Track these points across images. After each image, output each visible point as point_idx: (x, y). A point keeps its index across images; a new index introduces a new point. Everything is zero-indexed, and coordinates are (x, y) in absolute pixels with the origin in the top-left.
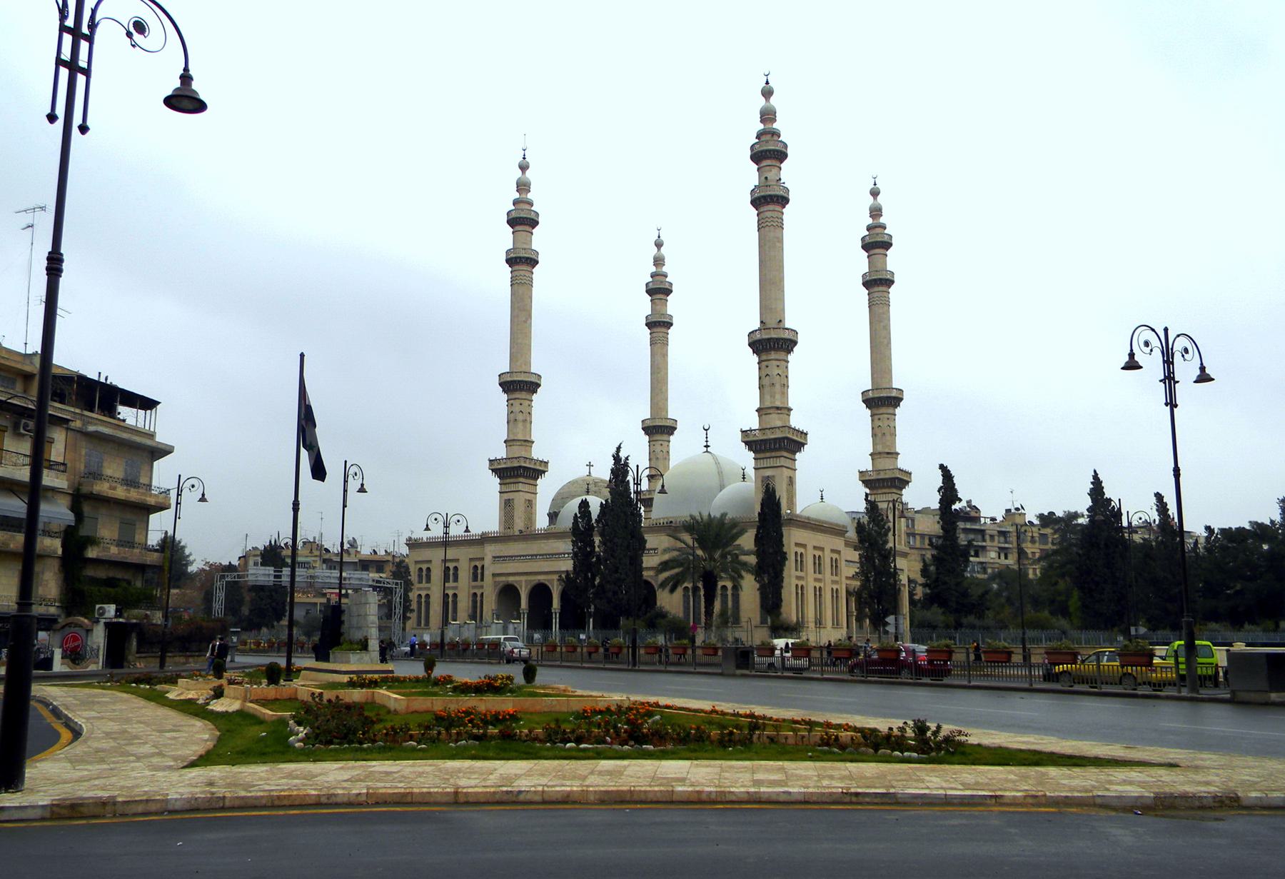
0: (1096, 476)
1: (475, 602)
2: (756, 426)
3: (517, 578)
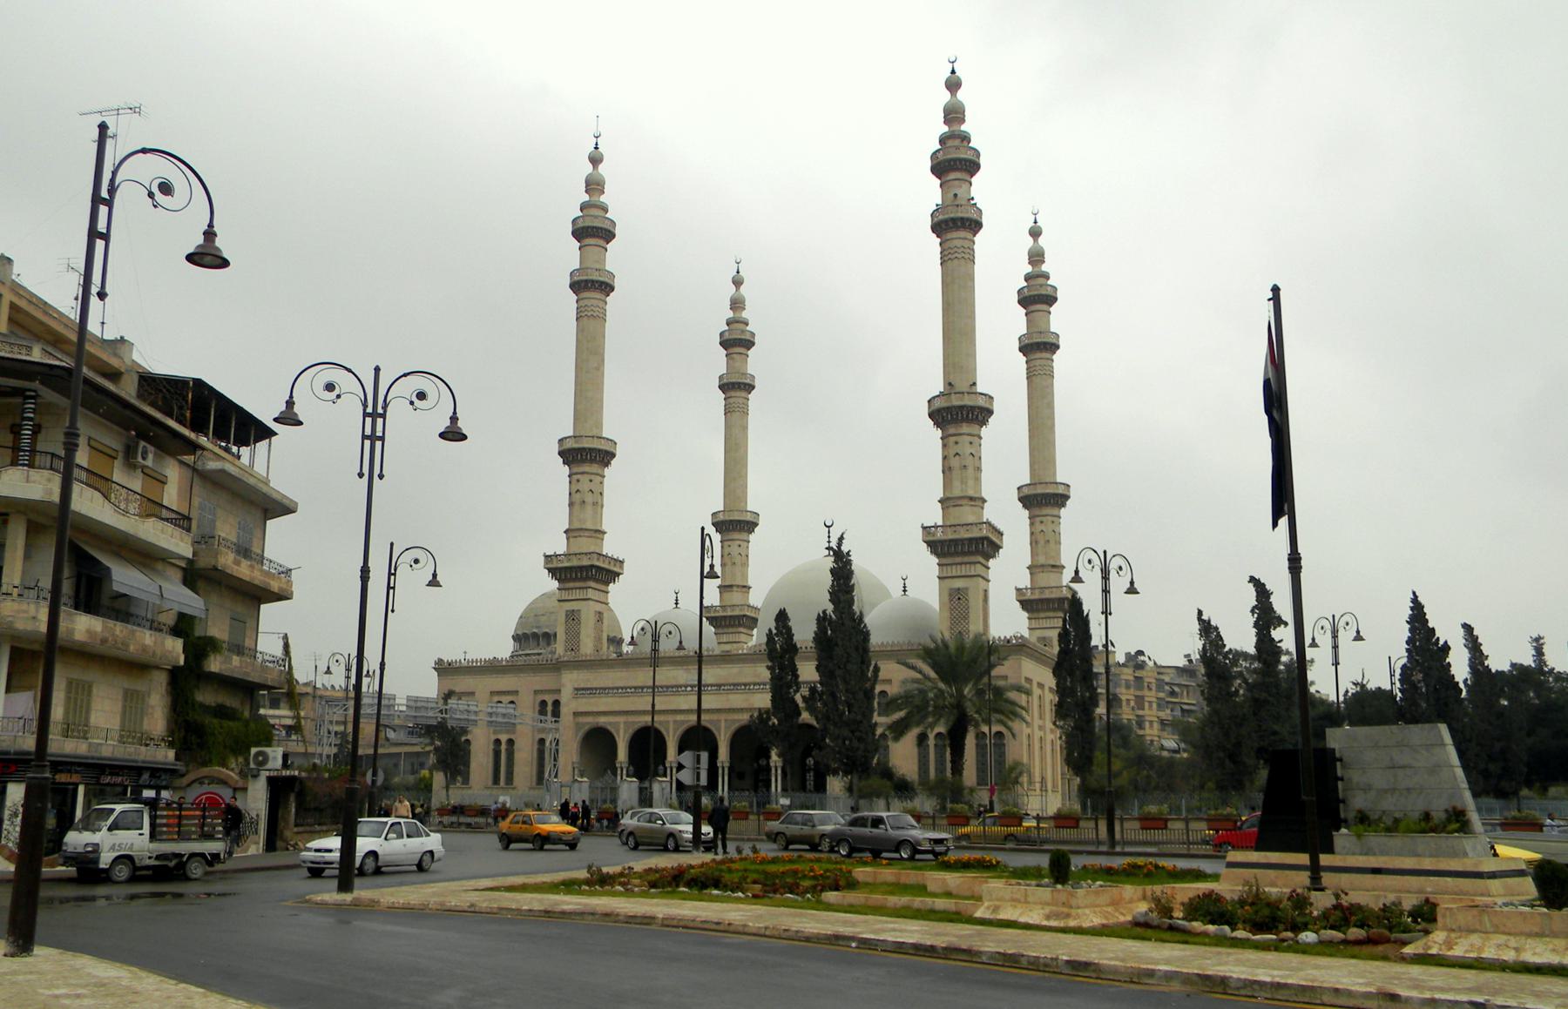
0: (1415, 600)
1: (497, 754)
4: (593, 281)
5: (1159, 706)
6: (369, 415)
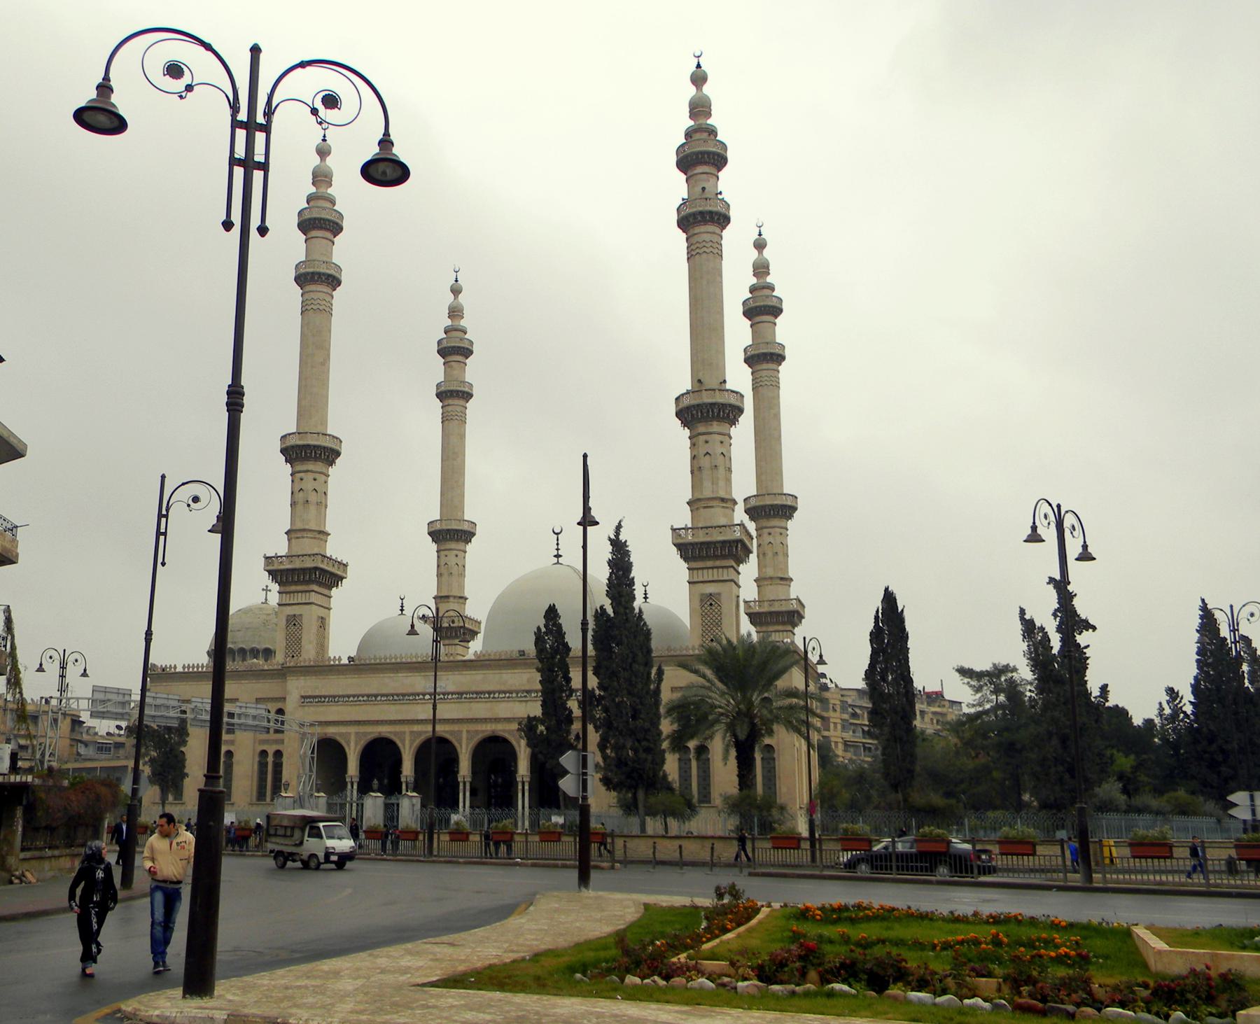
1: (263, 766)
2: (283, 550)
3: (343, 729)
4: (319, 274)
5: (843, 727)
6: (242, 125)
